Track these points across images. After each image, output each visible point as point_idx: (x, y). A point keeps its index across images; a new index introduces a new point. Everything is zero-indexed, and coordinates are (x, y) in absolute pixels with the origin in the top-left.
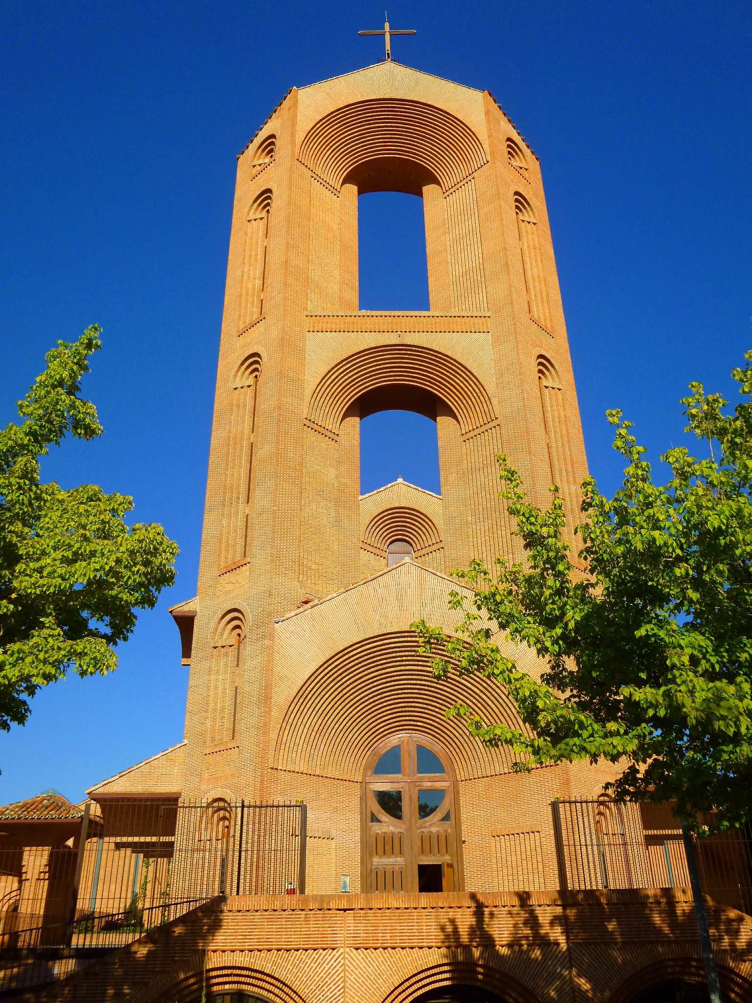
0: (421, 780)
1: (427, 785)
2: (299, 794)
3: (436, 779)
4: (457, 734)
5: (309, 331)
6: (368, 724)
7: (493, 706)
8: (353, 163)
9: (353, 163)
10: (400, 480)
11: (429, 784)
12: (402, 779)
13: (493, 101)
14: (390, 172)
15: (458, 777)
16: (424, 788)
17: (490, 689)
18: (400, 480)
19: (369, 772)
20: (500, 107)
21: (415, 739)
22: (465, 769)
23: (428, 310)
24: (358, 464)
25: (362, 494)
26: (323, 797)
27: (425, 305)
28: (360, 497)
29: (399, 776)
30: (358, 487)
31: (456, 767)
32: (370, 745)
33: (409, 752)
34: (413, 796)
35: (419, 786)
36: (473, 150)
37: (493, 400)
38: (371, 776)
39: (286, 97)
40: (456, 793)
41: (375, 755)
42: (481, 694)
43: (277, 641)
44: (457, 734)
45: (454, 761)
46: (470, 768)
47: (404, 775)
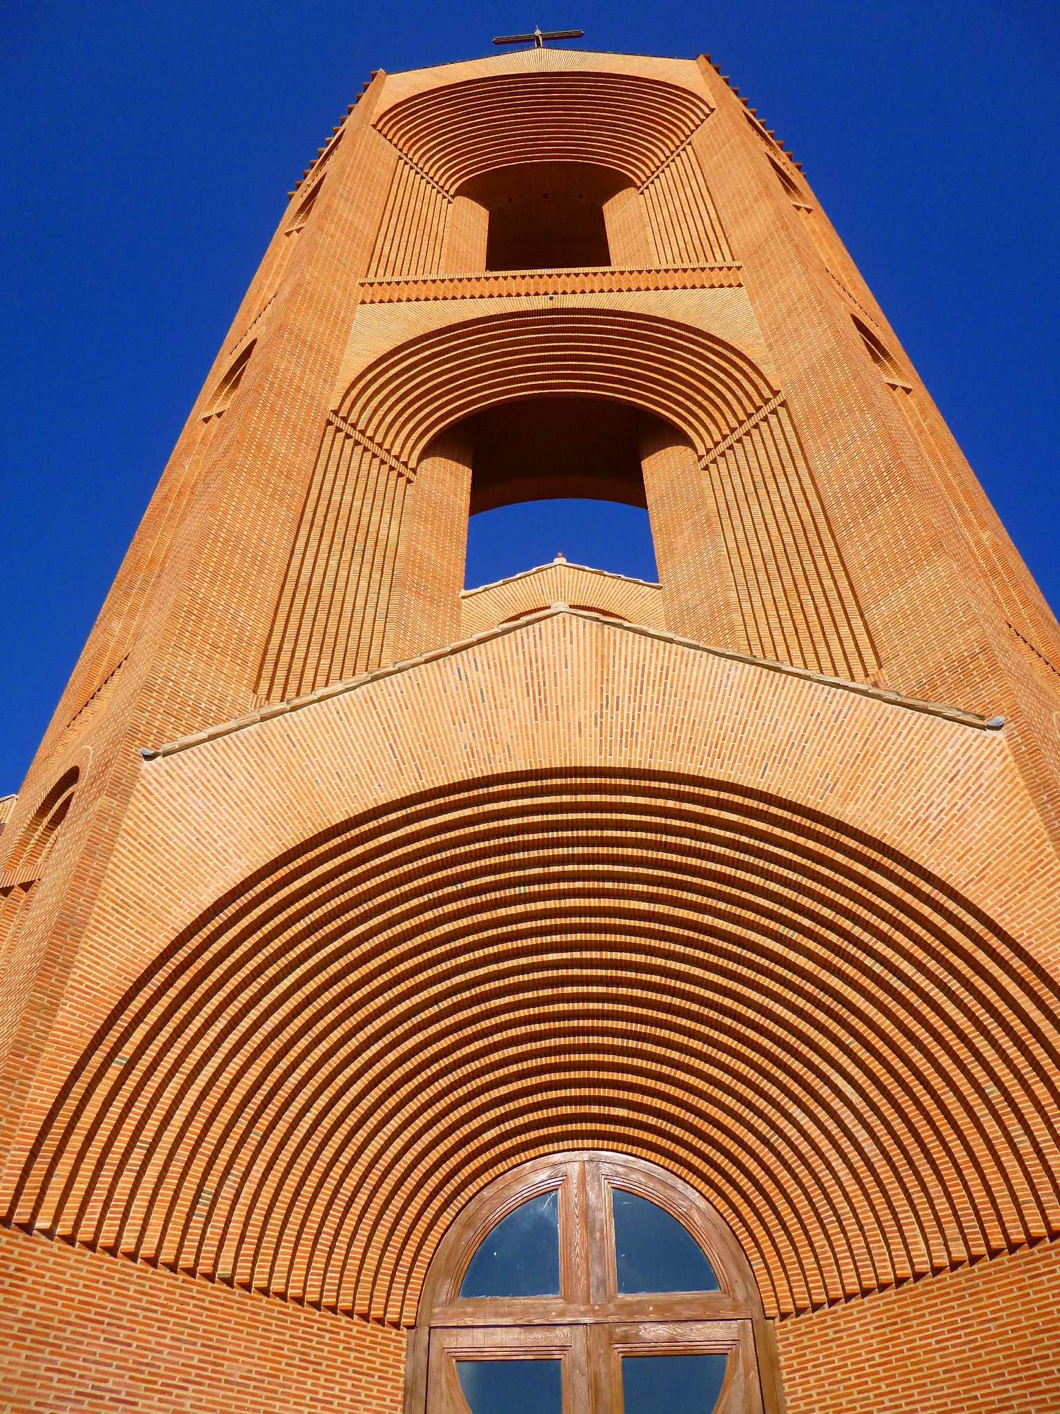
0: (633, 1315)
1: (655, 1333)
2: (118, 1350)
3: (687, 1314)
4: (750, 1139)
5: (363, 302)
6: (440, 1106)
7: (861, 1135)
8: (476, 170)
9: (476, 170)
10: (560, 560)
11: (662, 1331)
12: (562, 1313)
13: (713, 71)
14: (546, 196)
15: (770, 1303)
16: (641, 1349)
17: (845, 1144)
18: (560, 560)
19: (446, 1288)
20: (727, 81)
21: (605, 1168)
22: (794, 1269)
23: (608, 263)
24: (464, 537)
25: (467, 587)
26: (237, 1370)
27: (607, 263)
28: (464, 592)
29: (553, 1302)
30: (460, 572)
31: (758, 1265)
32: (449, 1188)
33: (586, 1211)
34: (604, 1384)
35: (625, 1340)
36: (759, 1232)
37: (764, 369)
38: (451, 1302)
39: (366, 87)
40: (767, 1365)
41: (467, 1225)
42: (824, 975)
43: (137, 803)
44: (750, 1139)
45: (748, 1243)
46: (809, 1262)
47: (568, 1299)
